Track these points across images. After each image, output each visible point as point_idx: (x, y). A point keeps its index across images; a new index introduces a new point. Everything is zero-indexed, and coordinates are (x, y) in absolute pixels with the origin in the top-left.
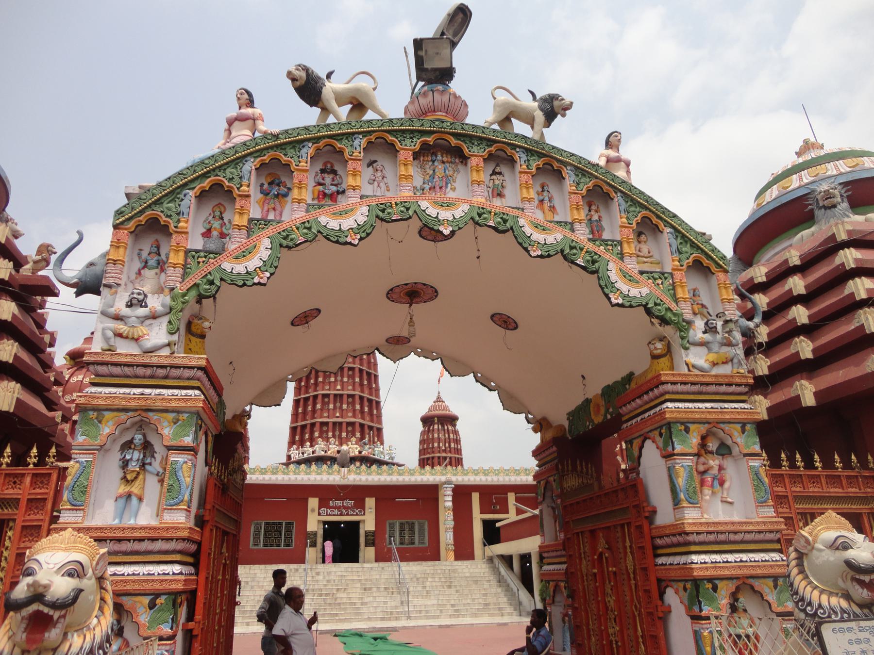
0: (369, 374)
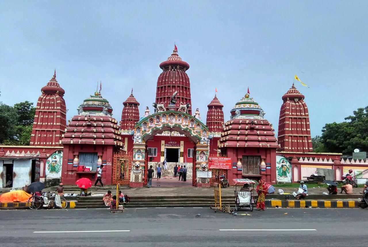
0: (186, 88)
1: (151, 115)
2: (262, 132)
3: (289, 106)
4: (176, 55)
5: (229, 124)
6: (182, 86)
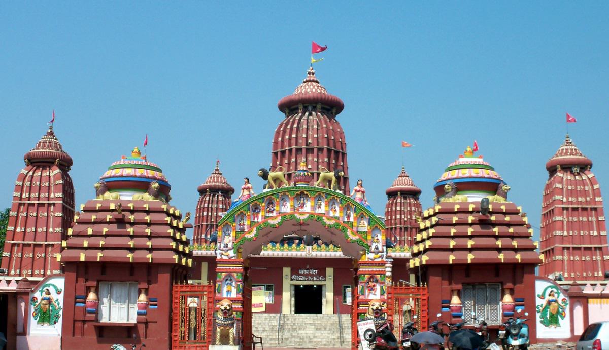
1: (255, 195)
2: (504, 229)
3: (561, 182)
4: (313, 81)
5: (432, 213)
6: (328, 149)
